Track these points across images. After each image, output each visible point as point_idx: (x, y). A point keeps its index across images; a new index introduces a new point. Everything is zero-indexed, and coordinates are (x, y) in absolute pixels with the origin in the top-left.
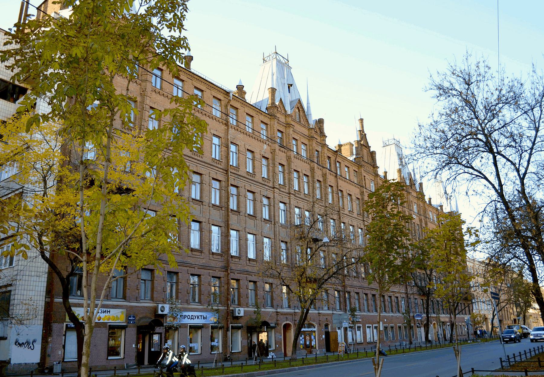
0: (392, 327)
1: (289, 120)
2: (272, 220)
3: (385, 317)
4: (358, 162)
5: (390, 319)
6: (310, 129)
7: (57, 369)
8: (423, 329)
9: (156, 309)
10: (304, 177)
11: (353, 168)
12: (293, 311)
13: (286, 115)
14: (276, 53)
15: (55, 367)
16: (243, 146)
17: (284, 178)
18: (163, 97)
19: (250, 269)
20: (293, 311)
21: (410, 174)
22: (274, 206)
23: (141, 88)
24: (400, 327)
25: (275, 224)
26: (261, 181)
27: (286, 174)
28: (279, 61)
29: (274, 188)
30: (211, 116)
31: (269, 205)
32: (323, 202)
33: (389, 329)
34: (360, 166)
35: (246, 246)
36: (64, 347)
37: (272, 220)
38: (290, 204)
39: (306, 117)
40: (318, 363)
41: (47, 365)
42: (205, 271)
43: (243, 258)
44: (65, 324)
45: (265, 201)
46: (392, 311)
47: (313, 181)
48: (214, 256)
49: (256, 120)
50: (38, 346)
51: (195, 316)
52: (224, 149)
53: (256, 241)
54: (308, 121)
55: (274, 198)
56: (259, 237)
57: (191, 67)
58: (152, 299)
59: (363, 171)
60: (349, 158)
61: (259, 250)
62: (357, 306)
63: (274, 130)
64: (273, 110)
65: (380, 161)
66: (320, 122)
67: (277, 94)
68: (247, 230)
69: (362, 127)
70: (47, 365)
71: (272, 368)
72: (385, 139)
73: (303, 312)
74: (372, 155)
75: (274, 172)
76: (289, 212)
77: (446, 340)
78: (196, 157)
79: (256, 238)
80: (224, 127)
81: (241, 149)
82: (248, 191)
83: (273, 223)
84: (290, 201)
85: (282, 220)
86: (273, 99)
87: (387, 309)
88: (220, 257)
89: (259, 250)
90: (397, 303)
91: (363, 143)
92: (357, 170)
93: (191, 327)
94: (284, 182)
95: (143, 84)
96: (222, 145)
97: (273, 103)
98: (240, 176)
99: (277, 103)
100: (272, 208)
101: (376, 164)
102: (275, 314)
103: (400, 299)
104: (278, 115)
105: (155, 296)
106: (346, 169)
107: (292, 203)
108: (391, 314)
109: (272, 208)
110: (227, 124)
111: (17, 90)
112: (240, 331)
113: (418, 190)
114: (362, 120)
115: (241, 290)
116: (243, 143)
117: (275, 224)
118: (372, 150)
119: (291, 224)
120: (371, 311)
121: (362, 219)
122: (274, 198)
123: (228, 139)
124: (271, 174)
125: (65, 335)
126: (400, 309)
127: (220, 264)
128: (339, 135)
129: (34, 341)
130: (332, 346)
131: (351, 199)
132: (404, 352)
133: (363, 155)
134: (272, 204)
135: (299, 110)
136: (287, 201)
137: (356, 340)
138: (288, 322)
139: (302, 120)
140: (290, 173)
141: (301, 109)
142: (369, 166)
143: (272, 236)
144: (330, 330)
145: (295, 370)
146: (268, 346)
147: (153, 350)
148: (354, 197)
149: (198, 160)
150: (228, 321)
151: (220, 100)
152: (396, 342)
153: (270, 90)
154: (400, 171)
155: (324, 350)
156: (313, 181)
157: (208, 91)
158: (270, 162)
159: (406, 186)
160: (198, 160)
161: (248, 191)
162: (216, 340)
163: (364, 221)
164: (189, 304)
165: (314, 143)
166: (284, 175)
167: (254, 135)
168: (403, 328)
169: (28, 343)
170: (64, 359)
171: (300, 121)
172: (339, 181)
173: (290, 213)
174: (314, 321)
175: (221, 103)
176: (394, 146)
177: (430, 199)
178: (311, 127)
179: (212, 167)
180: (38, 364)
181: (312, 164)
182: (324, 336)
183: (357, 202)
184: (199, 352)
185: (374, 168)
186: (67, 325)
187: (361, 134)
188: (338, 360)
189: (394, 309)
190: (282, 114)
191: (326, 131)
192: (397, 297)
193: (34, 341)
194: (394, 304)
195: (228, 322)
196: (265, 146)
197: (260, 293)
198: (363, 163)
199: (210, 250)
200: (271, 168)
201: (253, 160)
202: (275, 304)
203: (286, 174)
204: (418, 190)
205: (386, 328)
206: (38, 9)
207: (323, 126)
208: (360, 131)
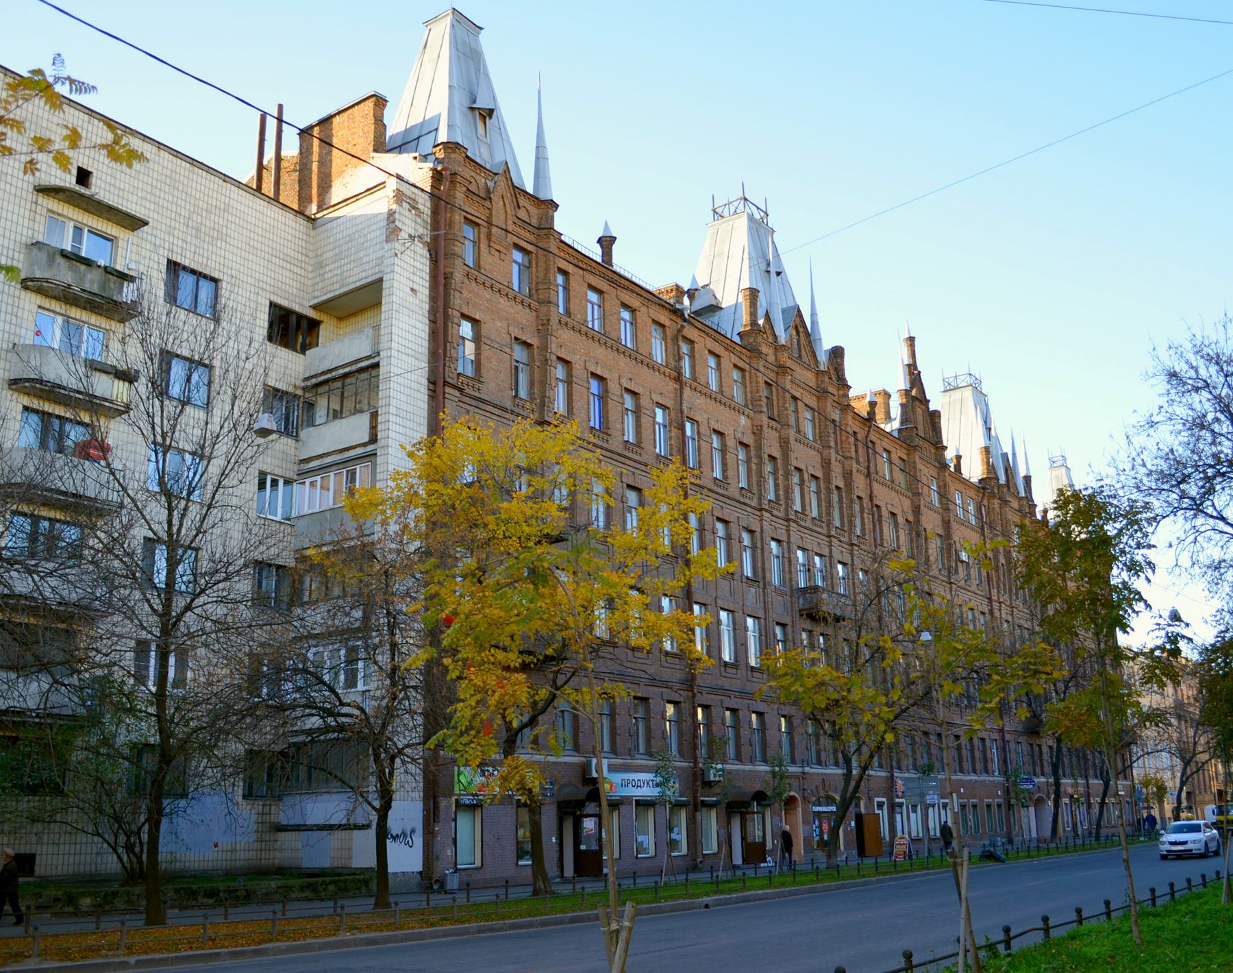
0: (975, 806)
1: (784, 358)
2: (760, 579)
3: (961, 783)
4: (906, 436)
5: (971, 788)
6: (819, 373)
7: (453, 882)
8: (1032, 810)
9: (585, 769)
10: (714, 437)
11: (899, 453)
12: (800, 770)
13: (778, 348)
14: (746, 199)
15: (449, 878)
16: (616, 381)
17: (776, 486)
18: (527, 310)
19: (725, 683)
20: (800, 770)
21: (1005, 456)
22: (762, 549)
23: (538, 317)
24: (989, 806)
25: (765, 588)
26: (737, 496)
27: (536, 370)
28: (751, 218)
29: (761, 510)
30: (584, 329)
31: (753, 548)
32: (755, 500)
33: (970, 810)
34: (911, 448)
35: (719, 634)
36: (455, 840)
37: (759, 578)
38: (789, 542)
39: (811, 347)
40: (900, 872)
41: (436, 876)
42: (656, 689)
43: (743, 666)
44: (454, 798)
45: (746, 537)
46: (975, 771)
47: (829, 491)
48: (729, 670)
49: (642, 315)
50: (418, 841)
51: (639, 784)
52: (675, 432)
53: (734, 624)
54: (815, 356)
55: (762, 531)
56: (739, 615)
57: (614, 261)
58: (577, 748)
59: (917, 460)
60: (882, 426)
61: (740, 646)
62: (786, 749)
63: (758, 382)
64: (755, 337)
65: (949, 435)
66: (837, 354)
67: (762, 299)
68: (720, 603)
69: (913, 355)
70: (436, 876)
71: (813, 882)
72: (949, 374)
73: (848, 776)
74: (934, 417)
75: (760, 474)
76: (787, 561)
77: (1076, 835)
78: (630, 455)
79: (734, 619)
80: (672, 385)
81: (702, 430)
82: (629, 486)
83: (761, 585)
84: (789, 536)
85: (775, 578)
86: (753, 314)
87: (965, 765)
88: (677, 661)
89: (740, 646)
90: (984, 752)
91: (915, 397)
92: (905, 457)
93: (639, 803)
94: (777, 496)
95: (543, 309)
96: (670, 424)
97: (754, 323)
98: (610, 451)
99: (761, 322)
100: (758, 550)
101: (941, 442)
102: (770, 776)
103: (988, 743)
104: (764, 349)
105: (581, 741)
106: (712, 362)
107: (792, 540)
108: (973, 777)
109: (758, 550)
110: (678, 378)
111: (304, 325)
112: (713, 813)
113: (1023, 494)
114: (911, 340)
115: (714, 728)
116: (706, 416)
117: (765, 588)
118: (932, 407)
119: (791, 586)
120: (904, 768)
121: (824, 531)
122: (762, 531)
123: (682, 412)
124: (754, 480)
125: (455, 820)
126: (989, 765)
127: (678, 676)
128: (872, 376)
129: (413, 831)
130: (869, 845)
131: (896, 524)
132: (1029, 857)
133: (916, 422)
134: (759, 545)
135: (798, 332)
136: (784, 537)
137: (910, 833)
138: (792, 793)
139: (803, 353)
140: (787, 475)
141: (801, 330)
142: (927, 445)
143: (761, 614)
144: (863, 810)
145: (870, 883)
146: (764, 844)
147: (583, 847)
148: (901, 520)
149: (635, 461)
150: (696, 791)
151: (663, 326)
152: (982, 839)
153: (748, 293)
154: (753, 294)
155: (855, 852)
156: (760, 458)
157: (643, 309)
158: (753, 453)
159: (1000, 486)
160: (635, 461)
161: (629, 486)
162: (676, 830)
163: (830, 536)
164: (633, 758)
165: (829, 406)
166: (776, 479)
167: (720, 398)
168: (994, 808)
169: (404, 834)
170: (456, 864)
171: (800, 356)
172: (875, 485)
173: (790, 562)
174: (836, 792)
175: (664, 332)
176: (968, 393)
177: (959, 458)
178: (822, 368)
179: (623, 460)
180: (421, 873)
181: (826, 452)
182: (853, 824)
183: (907, 527)
184: (652, 853)
185: (937, 448)
186: (457, 801)
187: (911, 374)
188: (928, 868)
189: (979, 766)
190: (770, 345)
191: (850, 375)
192: (983, 740)
193: (413, 831)
194: (977, 754)
195: (698, 794)
196: (743, 420)
197: (745, 733)
198: (917, 441)
199: (747, 663)
200: (754, 466)
201: (569, 381)
202: (798, 757)
203: (536, 370)
204: (1023, 494)
205: (963, 807)
206: (305, 133)
207: (842, 364)
208: (909, 365)
